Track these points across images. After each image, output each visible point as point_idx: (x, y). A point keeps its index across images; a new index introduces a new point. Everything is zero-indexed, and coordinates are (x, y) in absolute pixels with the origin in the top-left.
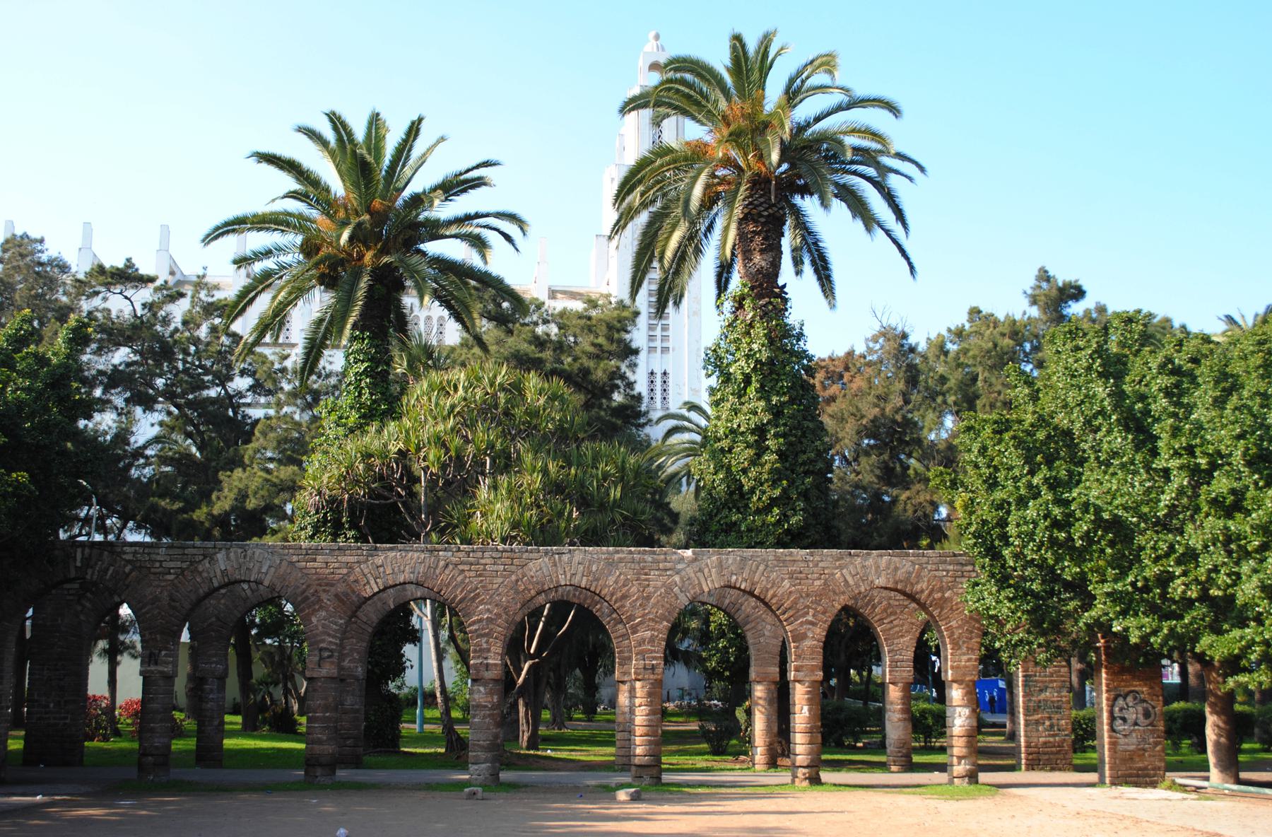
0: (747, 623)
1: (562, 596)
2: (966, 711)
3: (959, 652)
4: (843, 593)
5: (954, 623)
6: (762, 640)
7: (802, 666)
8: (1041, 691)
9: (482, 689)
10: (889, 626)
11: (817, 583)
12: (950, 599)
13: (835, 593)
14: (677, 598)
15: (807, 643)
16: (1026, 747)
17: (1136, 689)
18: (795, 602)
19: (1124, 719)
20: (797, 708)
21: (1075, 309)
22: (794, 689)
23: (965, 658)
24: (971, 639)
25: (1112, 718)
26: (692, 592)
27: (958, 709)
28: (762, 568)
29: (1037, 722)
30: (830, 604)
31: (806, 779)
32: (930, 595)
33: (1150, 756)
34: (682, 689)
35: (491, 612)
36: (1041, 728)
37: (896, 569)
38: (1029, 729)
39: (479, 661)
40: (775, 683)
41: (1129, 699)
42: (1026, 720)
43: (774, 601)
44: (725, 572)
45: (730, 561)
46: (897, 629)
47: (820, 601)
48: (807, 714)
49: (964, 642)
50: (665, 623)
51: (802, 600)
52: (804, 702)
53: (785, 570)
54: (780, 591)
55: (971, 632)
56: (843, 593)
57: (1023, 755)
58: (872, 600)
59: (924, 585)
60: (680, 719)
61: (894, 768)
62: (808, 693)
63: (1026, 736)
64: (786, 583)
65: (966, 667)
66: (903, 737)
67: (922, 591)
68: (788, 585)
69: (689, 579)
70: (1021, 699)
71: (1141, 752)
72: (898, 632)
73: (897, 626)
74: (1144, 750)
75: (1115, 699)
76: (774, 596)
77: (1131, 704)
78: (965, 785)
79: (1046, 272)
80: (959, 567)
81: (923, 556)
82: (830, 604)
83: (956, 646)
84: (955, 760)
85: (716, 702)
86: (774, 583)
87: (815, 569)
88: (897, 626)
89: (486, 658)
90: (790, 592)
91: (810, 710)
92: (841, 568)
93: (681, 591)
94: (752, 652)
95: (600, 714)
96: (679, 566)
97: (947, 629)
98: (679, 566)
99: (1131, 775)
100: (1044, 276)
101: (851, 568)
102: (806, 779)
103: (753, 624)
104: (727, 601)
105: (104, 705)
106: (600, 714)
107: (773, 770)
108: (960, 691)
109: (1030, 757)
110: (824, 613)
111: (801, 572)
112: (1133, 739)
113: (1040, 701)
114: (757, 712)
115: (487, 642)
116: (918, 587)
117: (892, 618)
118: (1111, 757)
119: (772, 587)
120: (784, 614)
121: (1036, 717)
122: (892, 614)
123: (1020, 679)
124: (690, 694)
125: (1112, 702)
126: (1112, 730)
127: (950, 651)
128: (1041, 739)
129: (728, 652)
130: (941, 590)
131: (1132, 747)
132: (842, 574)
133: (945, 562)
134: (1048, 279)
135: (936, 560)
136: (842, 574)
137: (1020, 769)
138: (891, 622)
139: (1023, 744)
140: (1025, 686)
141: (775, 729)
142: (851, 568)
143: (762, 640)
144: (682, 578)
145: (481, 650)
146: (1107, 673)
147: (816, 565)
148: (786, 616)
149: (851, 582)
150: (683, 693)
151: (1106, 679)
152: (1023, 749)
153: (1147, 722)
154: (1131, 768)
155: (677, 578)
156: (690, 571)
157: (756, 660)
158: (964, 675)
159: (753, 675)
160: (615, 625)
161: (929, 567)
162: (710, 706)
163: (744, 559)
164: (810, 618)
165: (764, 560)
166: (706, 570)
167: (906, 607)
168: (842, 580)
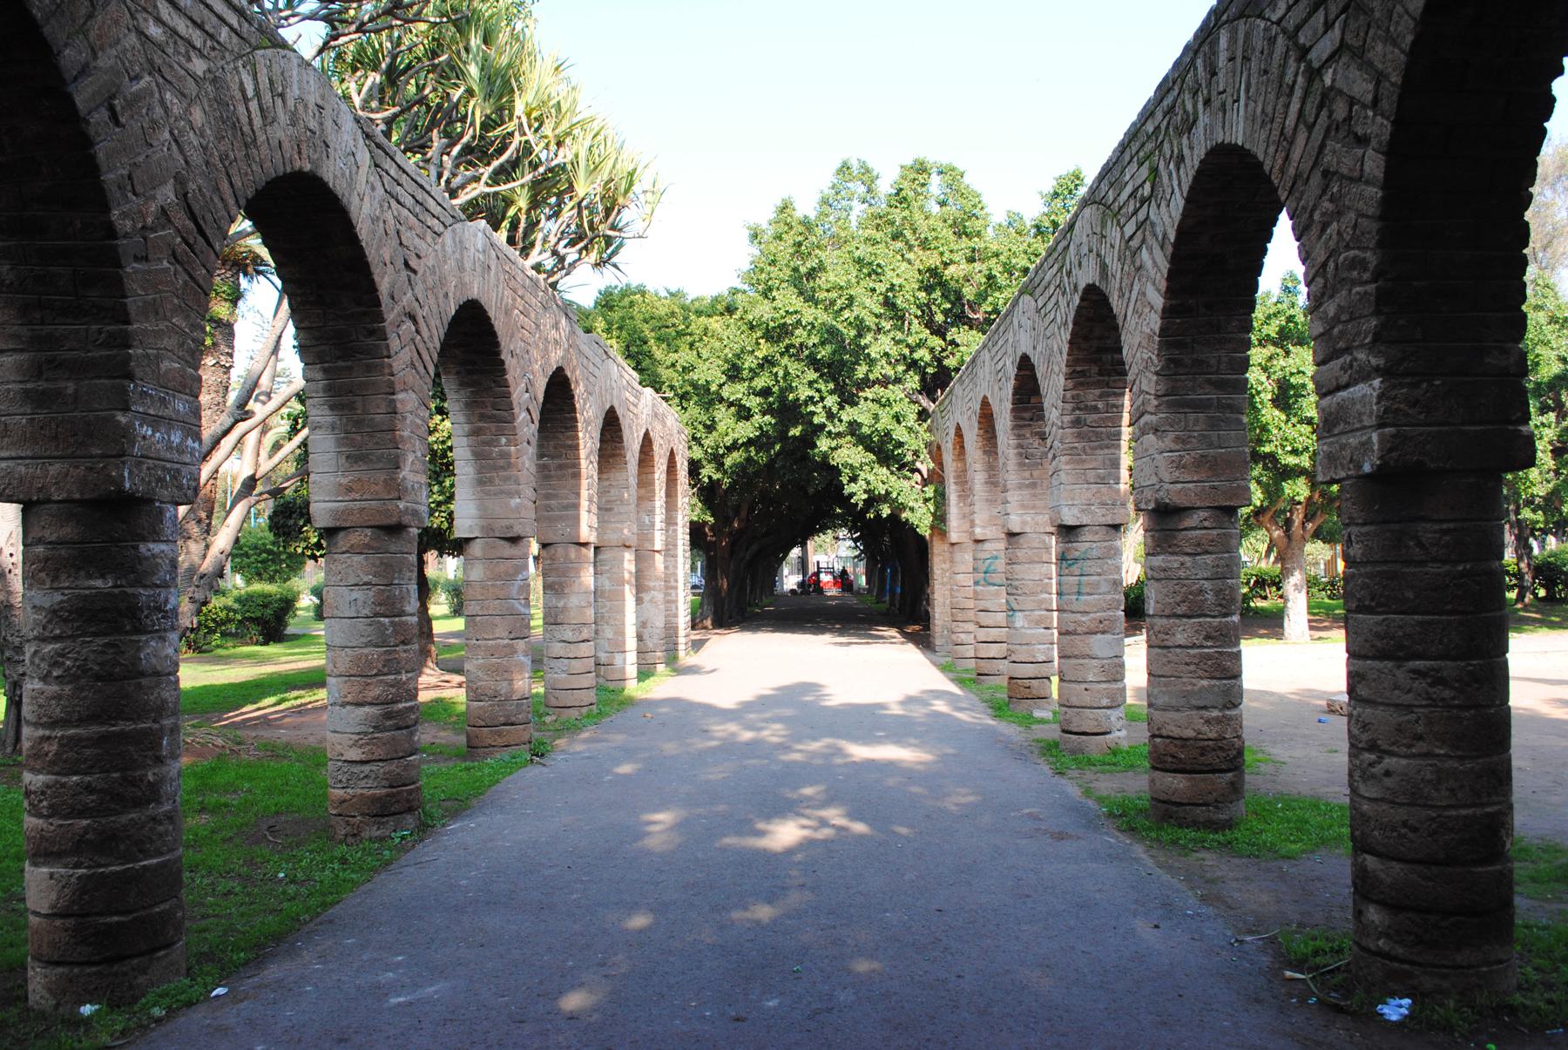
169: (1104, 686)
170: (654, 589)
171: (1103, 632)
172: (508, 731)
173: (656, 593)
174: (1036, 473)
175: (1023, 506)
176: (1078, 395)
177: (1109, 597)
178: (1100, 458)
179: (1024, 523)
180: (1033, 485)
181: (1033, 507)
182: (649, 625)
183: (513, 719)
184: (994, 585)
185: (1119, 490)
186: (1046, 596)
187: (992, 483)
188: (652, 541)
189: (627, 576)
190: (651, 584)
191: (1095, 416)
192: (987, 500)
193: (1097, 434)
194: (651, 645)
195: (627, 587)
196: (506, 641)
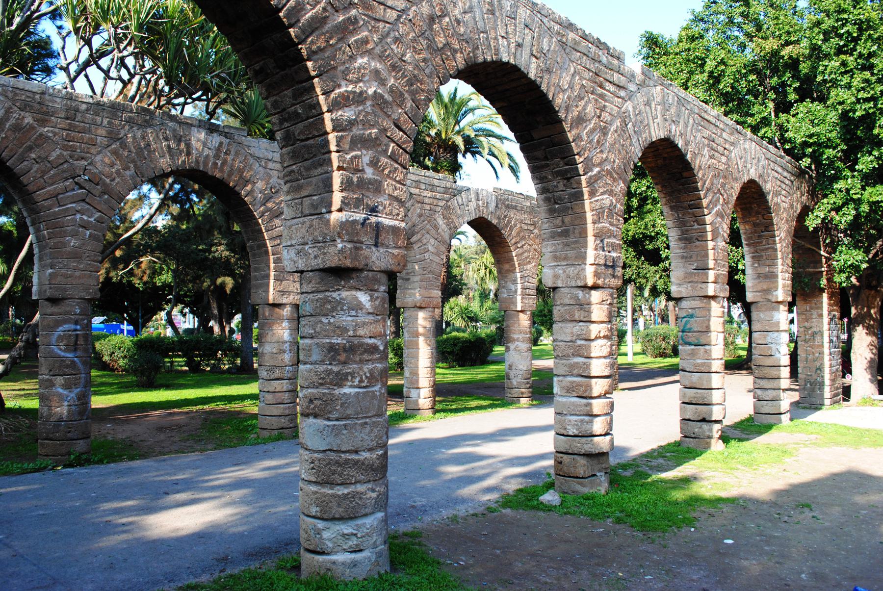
1: (197, 162)
9: (363, 298)
35: (382, 82)
39: (359, 216)
58: (509, 221)
88: (526, 251)
89: (373, 210)
115: (374, 163)
122: (523, 238)
145: (363, 184)
160: (271, 219)
169: (313, 488)
170: (518, 340)
171: (316, 416)
172: (48, 444)
173: (519, 344)
174: (567, 219)
175: (556, 258)
176: (276, 102)
177: (322, 368)
178: (314, 180)
179: (556, 276)
180: (565, 234)
181: (566, 258)
182: (514, 368)
183: (51, 436)
184: (690, 344)
185: (328, 221)
186: (581, 360)
187: (686, 239)
188: (515, 303)
189: (421, 330)
190: (515, 336)
191: (300, 126)
192: (683, 257)
193: (308, 147)
194: (515, 383)
195: (421, 339)
196: (47, 377)
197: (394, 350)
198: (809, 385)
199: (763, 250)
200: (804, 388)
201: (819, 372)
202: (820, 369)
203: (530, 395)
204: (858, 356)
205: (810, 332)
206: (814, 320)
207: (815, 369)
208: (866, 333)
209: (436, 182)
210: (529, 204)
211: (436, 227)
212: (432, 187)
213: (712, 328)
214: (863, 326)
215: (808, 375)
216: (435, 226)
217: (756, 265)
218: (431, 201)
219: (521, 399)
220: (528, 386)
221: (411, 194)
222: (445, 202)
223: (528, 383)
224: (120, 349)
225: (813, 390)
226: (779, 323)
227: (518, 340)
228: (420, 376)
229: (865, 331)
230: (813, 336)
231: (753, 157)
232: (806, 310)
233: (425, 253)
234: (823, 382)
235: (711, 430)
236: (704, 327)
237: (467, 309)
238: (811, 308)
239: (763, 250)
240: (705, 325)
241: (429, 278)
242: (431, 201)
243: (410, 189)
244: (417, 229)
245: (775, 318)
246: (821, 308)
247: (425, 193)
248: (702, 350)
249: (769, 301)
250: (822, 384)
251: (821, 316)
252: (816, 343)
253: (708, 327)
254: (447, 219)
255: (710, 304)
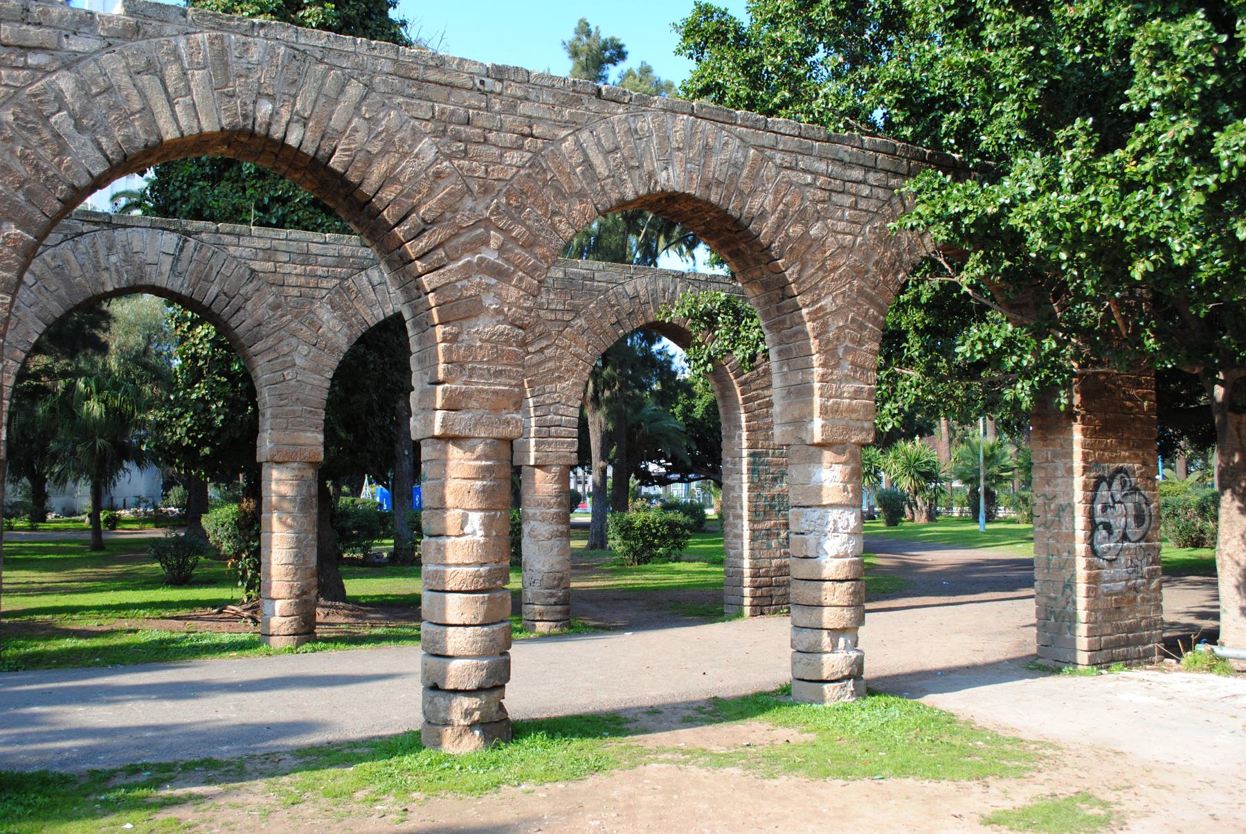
0: (257, 339)
2: (850, 519)
3: (837, 373)
4: (581, 195)
5: (826, 301)
6: (289, 374)
7: (466, 395)
8: (775, 479)
10: (536, 358)
11: (513, 158)
12: (820, 243)
13: (559, 192)
14: (62, 150)
15: (484, 326)
16: (752, 576)
17: (1125, 465)
18: (451, 205)
19: (1108, 527)
20: (452, 518)
21: (613, 73)
22: (443, 463)
23: (849, 388)
24: (860, 343)
25: (1092, 526)
26: (119, 135)
27: (834, 514)
28: (354, 90)
29: (769, 534)
30: (546, 222)
31: (472, 726)
32: (779, 226)
33: (1143, 599)
34: (139, 497)
36: (774, 543)
37: (707, 150)
38: (757, 545)
40: (313, 464)
41: (1116, 485)
42: (753, 530)
43: (388, 194)
44: (237, 85)
45: (255, 55)
46: (551, 365)
47: (521, 209)
48: (479, 536)
49: (847, 350)
50: (13, 230)
51: (468, 202)
52: (472, 502)
53: (423, 110)
54: (408, 168)
55: (862, 327)
56: (581, 195)
57: (747, 591)
59: (768, 202)
60: (135, 526)
61: (542, 627)
62: (483, 473)
63: (753, 557)
64: (427, 148)
65: (851, 410)
66: (558, 567)
67: (763, 215)
68: (431, 155)
69: (108, 90)
70: (745, 495)
71: (1132, 595)
72: (552, 371)
73: (551, 359)
74: (1135, 589)
75: (1096, 487)
76: (389, 179)
77: (1118, 497)
78: (848, 699)
79: (587, 25)
80: (835, 169)
81: (766, 129)
82: (546, 222)
83: (829, 352)
84: (826, 639)
85: (172, 509)
86: (389, 142)
87: (509, 120)
88: (551, 359)
90: (438, 175)
91: (488, 525)
92: (575, 126)
93: (79, 127)
94: (265, 397)
95: (51, 522)
96: (77, 44)
97: (814, 316)
98: (77, 44)
99: (1117, 644)
100: (584, 29)
101: (601, 128)
102: (472, 726)
103: (270, 341)
104: (214, 290)
105: (236, 506)
106: (51, 522)
107: (308, 646)
108: (838, 468)
109: (759, 593)
110: (529, 246)
111: (468, 122)
112: (1121, 570)
113: (773, 498)
114: (276, 526)
116: (754, 204)
117: (544, 343)
118: (1091, 609)
119: (384, 152)
120: (418, 235)
121: (768, 524)
122: (541, 336)
123: (745, 461)
124: (146, 501)
125: (1092, 489)
126: (1093, 551)
127: (818, 371)
128: (774, 562)
129: (208, 410)
130: (802, 217)
131: (1120, 586)
132: (578, 145)
133: (808, 152)
134: (588, 34)
135: (792, 143)
136: (578, 145)
137: (740, 615)
138: (541, 350)
139: (747, 572)
140: (752, 471)
141: (313, 561)
142: (601, 128)
143: (289, 374)
144: (81, 85)
146: (1084, 434)
147: (511, 108)
148: (423, 243)
149: (602, 170)
150: (139, 502)
151: (1084, 446)
152: (747, 581)
153: (1140, 531)
154: (1118, 629)
155: (65, 82)
156: (114, 65)
157: (274, 417)
158: (848, 429)
159: (266, 444)
161: (778, 157)
162: (167, 513)
163: (298, 55)
164: (491, 256)
165: (361, 69)
166: (172, 72)
167: (567, 324)
168: (577, 158)
197: (622, 530)
198: (1053, 620)
199: (790, 337)
200: (1045, 625)
201: (1068, 591)
202: (1070, 585)
203: (558, 617)
204: (1226, 558)
205: (1053, 506)
206: (1060, 481)
207: (1061, 586)
208: (1239, 508)
209: (314, 248)
210: (561, 275)
211: (315, 325)
212: (306, 258)
213: (450, 501)
214: (1234, 492)
215: (1050, 598)
216: (312, 323)
217: (786, 369)
218: (302, 280)
219: (537, 624)
220: (553, 600)
221: (253, 271)
222: (337, 281)
223: (552, 595)
224: (223, 526)
225: (1059, 631)
226: (820, 488)
227: (534, 517)
228: (273, 579)
229: (1237, 503)
230: (1058, 515)
231: (608, 145)
232: (1047, 461)
233: (284, 370)
234: (1075, 614)
235: (448, 709)
236: (436, 500)
237: (918, 460)
238: (1055, 455)
239: (790, 337)
240: (437, 494)
241: (294, 411)
242: (302, 280)
243: (251, 263)
244: (264, 330)
245: (814, 479)
246: (1069, 455)
247: (288, 268)
248: (434, 546)
249: (803, 442)
250: (1073, 618)
251: (1070, 471)
252: (1064, 530)
253: (442, 499)
254: (340, 308)
255: (446, 452)
